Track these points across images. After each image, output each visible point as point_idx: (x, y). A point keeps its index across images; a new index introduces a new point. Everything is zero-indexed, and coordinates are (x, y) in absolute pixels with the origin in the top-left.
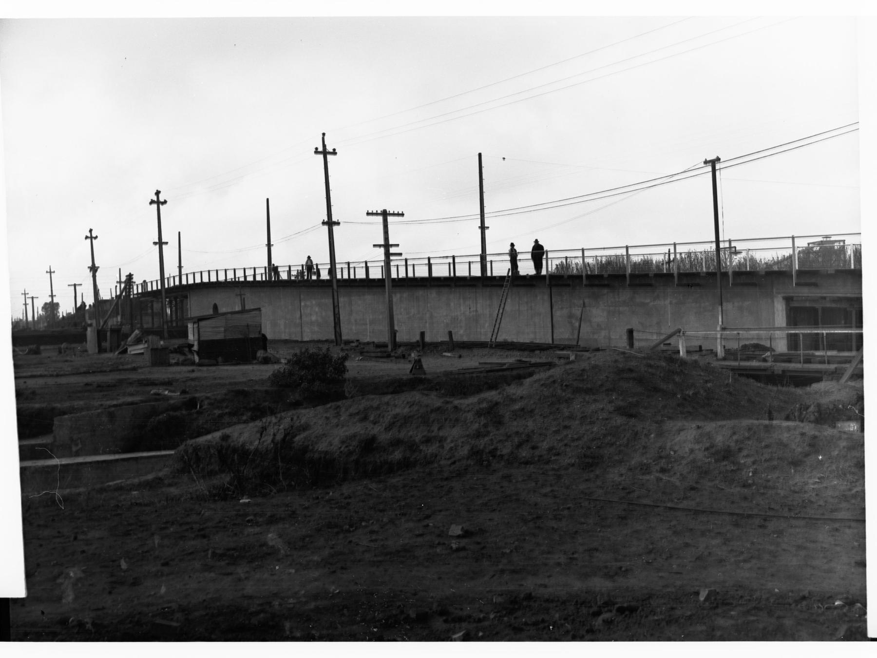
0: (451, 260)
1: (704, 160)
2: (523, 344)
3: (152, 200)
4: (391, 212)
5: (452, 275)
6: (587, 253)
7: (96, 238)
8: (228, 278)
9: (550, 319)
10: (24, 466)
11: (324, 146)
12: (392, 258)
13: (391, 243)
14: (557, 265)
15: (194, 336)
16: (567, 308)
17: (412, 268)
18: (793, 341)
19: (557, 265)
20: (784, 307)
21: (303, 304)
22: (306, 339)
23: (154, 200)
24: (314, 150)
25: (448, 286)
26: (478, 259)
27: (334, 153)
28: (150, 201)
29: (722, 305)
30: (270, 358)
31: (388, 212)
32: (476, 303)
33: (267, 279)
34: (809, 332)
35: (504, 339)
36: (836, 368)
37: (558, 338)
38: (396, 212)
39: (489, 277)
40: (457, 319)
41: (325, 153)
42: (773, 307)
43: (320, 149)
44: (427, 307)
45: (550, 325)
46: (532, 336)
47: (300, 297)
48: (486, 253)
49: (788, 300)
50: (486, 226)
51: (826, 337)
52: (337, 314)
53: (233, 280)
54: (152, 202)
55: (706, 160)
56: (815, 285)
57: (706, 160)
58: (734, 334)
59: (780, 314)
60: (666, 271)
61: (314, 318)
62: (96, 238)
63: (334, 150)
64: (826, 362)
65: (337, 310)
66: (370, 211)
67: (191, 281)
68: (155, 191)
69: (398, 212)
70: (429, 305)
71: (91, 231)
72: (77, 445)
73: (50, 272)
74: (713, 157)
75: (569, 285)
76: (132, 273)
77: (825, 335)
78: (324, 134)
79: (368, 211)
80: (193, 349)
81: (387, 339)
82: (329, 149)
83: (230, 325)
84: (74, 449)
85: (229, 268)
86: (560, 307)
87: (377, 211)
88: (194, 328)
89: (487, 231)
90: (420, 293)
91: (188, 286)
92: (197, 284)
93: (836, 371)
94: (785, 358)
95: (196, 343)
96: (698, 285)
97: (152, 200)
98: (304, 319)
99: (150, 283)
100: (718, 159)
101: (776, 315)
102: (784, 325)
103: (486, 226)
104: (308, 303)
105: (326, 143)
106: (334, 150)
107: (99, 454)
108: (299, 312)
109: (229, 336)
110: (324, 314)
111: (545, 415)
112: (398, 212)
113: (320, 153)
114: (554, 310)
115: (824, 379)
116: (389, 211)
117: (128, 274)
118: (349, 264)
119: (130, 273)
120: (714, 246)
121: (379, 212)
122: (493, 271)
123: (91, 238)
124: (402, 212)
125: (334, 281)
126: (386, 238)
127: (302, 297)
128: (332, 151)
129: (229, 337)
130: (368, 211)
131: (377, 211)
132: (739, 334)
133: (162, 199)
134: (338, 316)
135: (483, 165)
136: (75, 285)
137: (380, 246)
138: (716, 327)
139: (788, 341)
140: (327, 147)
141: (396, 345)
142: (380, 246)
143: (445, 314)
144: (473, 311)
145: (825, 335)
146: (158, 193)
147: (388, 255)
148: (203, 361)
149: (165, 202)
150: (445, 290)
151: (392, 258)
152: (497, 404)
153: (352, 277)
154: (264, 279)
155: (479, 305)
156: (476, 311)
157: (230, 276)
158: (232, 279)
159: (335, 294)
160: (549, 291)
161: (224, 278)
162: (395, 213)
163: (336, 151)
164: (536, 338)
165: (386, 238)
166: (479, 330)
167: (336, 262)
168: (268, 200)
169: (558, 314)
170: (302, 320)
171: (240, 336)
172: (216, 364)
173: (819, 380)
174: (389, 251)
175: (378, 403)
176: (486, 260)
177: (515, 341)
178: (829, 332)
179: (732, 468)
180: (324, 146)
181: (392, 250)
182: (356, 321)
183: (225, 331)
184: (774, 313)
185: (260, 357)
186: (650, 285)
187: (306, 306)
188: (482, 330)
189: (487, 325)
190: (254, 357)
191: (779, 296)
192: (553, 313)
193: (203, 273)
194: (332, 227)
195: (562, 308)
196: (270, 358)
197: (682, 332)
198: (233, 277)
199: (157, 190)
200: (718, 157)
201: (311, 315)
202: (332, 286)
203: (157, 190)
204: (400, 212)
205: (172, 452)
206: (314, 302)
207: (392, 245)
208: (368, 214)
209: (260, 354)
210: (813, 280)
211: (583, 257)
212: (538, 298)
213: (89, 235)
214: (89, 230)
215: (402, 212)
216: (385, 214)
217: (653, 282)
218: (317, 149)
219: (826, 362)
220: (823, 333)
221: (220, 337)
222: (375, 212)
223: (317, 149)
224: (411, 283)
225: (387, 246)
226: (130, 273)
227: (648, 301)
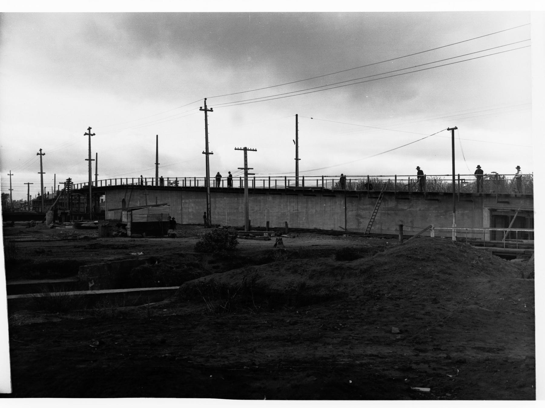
0: (184, 179)
1: (447, 128)
2: (327, 231)
3: (86, 133)
4: (249, 149)
5: (184, 186)
6: (398, 178)
7: (44, 154)
8: (134, 182)
9: (344, 217)
10: (9, 298)
11: (206, 106)
12: (249, 176)
13: (88, 161)
14: (336, 183)
15: (127, 219)
16: (355, 211)
17: (189, 183)
18: (493, 234)
19: (336, 183)
20: (489, 215)
21: (183, 201)
22: (184, 223)
23: (87, 133)
24: (200, 108)
25: (280, 194)
26: (295, 178)
27: (211, 110)
28: (85, 133)
29: (455, 213)
30: (176, 234)
31: (247, 149)
32: (298, 206)
33: (159, 185)
34: (502, 230)
35: (315, 228)
36: (524, 251)
37: (349, 228)
38: (252, 149)
39: (166, 187)
40: (285, 214)
41: (206, 110)
42: (482, 214)
43: (203, 108)
44: (266, 206)
45: (344, 220)
46: (308, 226)
47: (182, 197)
48: (298, 175)
49: (492, 210)
50: (299, 158)
51: (518, 233)
52: (209, 209)
53: (138, 184)
54: (86, 134)
55: (449, 128)
56: (508, 203)
57: (449, 128)
58: (465, 230)
59: (486, 218)
60: (357, 189)
61: (190, 210)
62: (44, 154)
63: (212, 109)
64: (517, 248)
65: (209, 205)
66: (237, 148)
67: (104, 185)
68: (88, 128)
69: (253, 149)
70: (267, 205)
71: (41, 150)
72: (91, 283)
73: (10, 175)
74: (454, 127)
75: (357, 197)
76: (71, 178)
77: (517, 232)
78: (206, 99)
79: (236, 148)
80: (126, 227)
81: (266, 225)
82: (209, 108)
83: (151, 214)
84: (90, 285)
85: (135, 178)
86: (351, 209)
87: (241, 148)
88: (127, 214)
89: (299, 161)
90: (261, 198)
91: (102, 188)
92: (103, 187)
93: (524, 253)
94: (479, 243)
95: (129, 224)
96: (437, 200)
97: (86, 133)
98: (184, 210)
99: (80, 185)
100: (456, 128)
101: (484, 220)
102: (489, 226)
103: (299, 158)
104: (187, 201)
105: (207, 104)
106: (212, 109)
107: (103, 289)
108: (181, 207)
109: (150, 220)
110: (197, 208)
111: (403, 273)
112: (253, 149)
113: (203, 110)
114: (347, 211)
115: (517, 258)
116: (248, 148)
117: (68, 178)
118: (195, 178)
119: (69, 178)
120: (451, 178)
121: (242, 148)
122: (224, 185)
123: (41, 154)
124: (256, 149)
125: (208, 188)
126: (246, 164)
127: (183, 197)
128: (210, 109)
129: (150, 221)
130: (236, 148)
131: (241, 148)
132: (467, 230)
133: (92, 133)
134: (209, 210)
135: (209, 141)
136: (28, 184)
137: (242, 169)
138: (452, 225)
139: (490, 235)
140: (207, 107)
141: (250, 228)
142: (242, 169)
143: (277, 211)
144: (296, 210)
145: (517, 232)
146: (89, 129)
147: (246, 174)
148: (134, 235)
149: (94, 134)
150: (278, 197)
151: (249, 176)
152: (373, 266)
153: (196, 185)
154: (154, 184)
155: (299, 207)
156: (298, 210)
157: (108, 183)
158: (137, 183)
159: (209, 196)
160: (344, 199)
161: (132, 182)
162: (242, 149)
163: (213, 110)
164: (335, 228)
165: (246, 164)
166: (299, 222)
167: (210, 177)
168: (157, 136)
169: (349, 214)
170: (183, 211)
171: (157, 221)
172: (143, 237)
173: (514, 258)
174: (247, 172)
175: (300, 263)
176: (298, 179)
177: (322, 229)
178: (493, 230)
179: (515, 303)
180: (206, 106)
181: (249, 171)
182: (218, 213)
183: (148, 217)
184: (482, 218)
185: (170, 233)
186: (408, 199)
187: (186, 203)
188: (301, 222)
189: (304, 218)
190: (166, 234)
191: (486, 208)
192: (347, 213)
193: (117, 180)
194: (208, 155)
195: (352, 210)
196: (176, 234)
197: (432, 228)
198: (110, 184)
199: (89, 127)
200: (456, 127)
201: (189, 208)
202: (207, 192)
203: (89, 127)
204: (255, 149)
205: (178, 287)
206: (191, 201)
207: (249, 169)
208: (236, 149)
209: (170, 231)
210: (507, 200)
211: (396, 180)
212: (337, 204)
213: (39, 152)
214: (39, 149)
215: (256, 149)
216: (245, 150)
217: (410, 197)
218: (201, 108)
219: (517, 248)
220: (516, 231)
221: (145, 220)
222: (240, 148)
223: (201, 108)
224: (255, 191)
225: (246, 169)
226: (69, 178)
227: (406, 208)
